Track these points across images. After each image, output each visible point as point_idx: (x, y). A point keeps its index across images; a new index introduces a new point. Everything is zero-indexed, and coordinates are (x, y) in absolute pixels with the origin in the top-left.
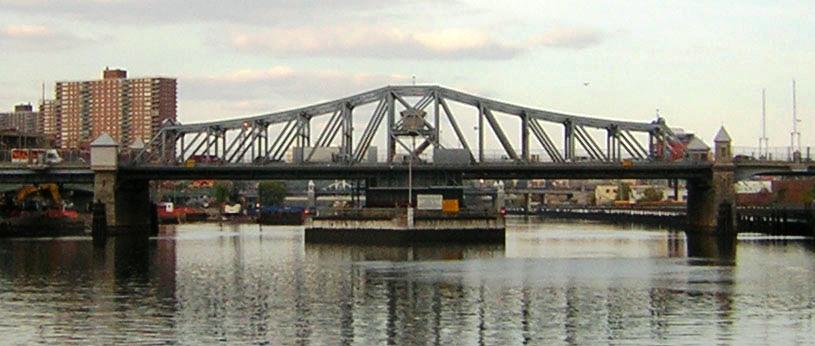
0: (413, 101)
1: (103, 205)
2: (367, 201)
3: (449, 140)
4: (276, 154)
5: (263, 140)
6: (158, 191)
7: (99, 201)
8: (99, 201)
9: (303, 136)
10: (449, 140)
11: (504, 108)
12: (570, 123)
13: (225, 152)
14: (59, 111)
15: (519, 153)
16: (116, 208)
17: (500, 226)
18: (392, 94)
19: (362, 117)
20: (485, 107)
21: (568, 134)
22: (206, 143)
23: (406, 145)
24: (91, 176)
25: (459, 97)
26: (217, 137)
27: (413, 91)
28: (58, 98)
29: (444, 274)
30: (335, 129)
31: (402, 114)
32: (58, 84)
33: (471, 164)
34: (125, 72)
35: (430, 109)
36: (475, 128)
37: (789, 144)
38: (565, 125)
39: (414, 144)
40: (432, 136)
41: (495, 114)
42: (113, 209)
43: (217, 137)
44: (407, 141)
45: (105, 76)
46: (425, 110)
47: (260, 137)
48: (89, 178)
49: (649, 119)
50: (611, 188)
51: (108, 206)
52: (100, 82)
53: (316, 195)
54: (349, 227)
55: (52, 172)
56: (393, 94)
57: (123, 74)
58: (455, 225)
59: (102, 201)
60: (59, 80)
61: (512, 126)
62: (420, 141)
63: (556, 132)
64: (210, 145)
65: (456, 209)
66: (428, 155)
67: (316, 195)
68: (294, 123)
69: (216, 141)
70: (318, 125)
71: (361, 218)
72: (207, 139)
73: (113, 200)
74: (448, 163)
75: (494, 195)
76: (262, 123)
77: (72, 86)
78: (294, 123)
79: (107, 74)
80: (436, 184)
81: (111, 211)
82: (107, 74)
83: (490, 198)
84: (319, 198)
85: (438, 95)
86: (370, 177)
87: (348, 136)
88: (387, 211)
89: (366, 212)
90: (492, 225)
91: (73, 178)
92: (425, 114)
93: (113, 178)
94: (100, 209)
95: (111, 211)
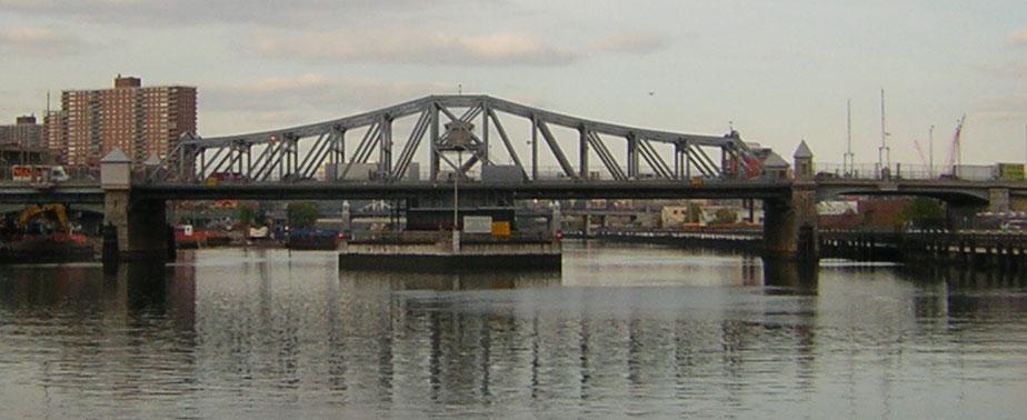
0: (459, 112)
3: (499, 155)
5: (292, 155)
7: (110, 223)
8: (110, 223)
9: (337, 152)
10: (499, 155)
11: (560, 120)
12: (634, 136)
13: (250, 169)
15: (577, 170)
16: (129, 230)
17: (556, 251)
19: (402, 130)
20: (539, 119)
23: (451, 161)
24: (102, 196)
25: (510, 108)
26: (241, 152)
27: (458, 101)
28: (64, 109)
31: (447, 126)
32: (65, 93)
34: (139, 80)
35: (478, 121)
38: (629, 139)
39: (460, 160)
40: (481, 151)
42: (126, 232)
43: (241, 152)
44: (453, 157)
45: (117, 85)
46: (472, 122)
47: (289, 152)
48: (99, 198)
49: (721, 132)
53: (352, 217)
54: (388, 252)
55: (58, 191)
56: (436, 104)
57: (136, 82)
58: (506, 250)
60: (65, 89)
61: (569, 140)
62: (466, 157)
63: (618, 147)
64: (234, 161)
65: (507, 232)
66: (476, 171)
67: (352, 217)
68: (326, 136)
70: (353, 139)
71: (401, 243)
72: (230, 155)
73: (125, 222)
74: (498, 182)
75: (550, 217)
76: (292, 137)
77: (81, 95)
78: (326, 136)
79: (119, 82)
80: (485, 205)
81: (123, 235)
82: (119, 82)
83: (544, 219)
85: (487, 105)
88: (431, 235)
90: (547, 250)
91: (82, 198)
93: (125, 198)
94: (111, 234)
95: (123, 235)
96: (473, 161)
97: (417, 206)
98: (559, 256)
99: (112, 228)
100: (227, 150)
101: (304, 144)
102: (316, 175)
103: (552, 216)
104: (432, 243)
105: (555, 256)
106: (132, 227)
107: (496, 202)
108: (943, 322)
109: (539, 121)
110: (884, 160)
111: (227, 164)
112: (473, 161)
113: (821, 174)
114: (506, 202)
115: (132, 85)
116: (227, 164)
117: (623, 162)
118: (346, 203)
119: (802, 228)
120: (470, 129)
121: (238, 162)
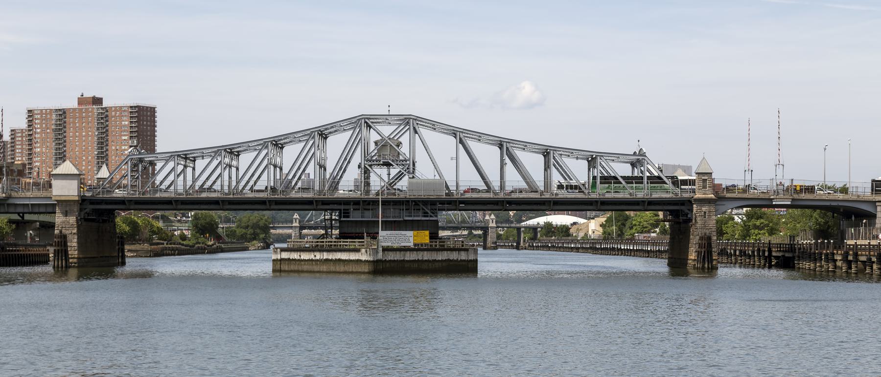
0: (387, 130)
1: (65, 237)
2: (340, 233)
3: (425, 171)
4: (230, 182)
5: (234, 169)
6: (122, 220)
7: (61, 232)
8: (61, 232)
9: (275, 166)
10: (425, 171)
11: (479, 137)
12: (548, 153)
13: (238, 182)
14: (30, 140)
15: (541, 185)
16: (78, 239)
17: (471, 257)
18: (366, 122)
19: (336, 144)
20: (460, 136)
21: (547, 167)
22: (172, 175)
23: (379, 178)
24: (54, 205)
25: (433, 125)
26: (185, 166)
27: (386, 119)
28: (29, 126)
29: (246, 195)
30: (307, 160)
31: (376, 143)
32: (30, 111)
33: (447, 194)
34: (101, 99)
35: (405, 139)
36: (452, 159)
37: (267, 185)
38: (545, 156)
39: (389, 174)
40: (409, 167)
41: (472, 144)
42: (76, 240)
43: (185, 166)
44: (383, 171)
45: (79, 104)
46: (400, 140)
47: (230, 166)
48: (50, 209)
49: (630, 149)
50: (341, 192)
51: (69, 237)
52: (74, 109)
53: (302, 228)
54: (318, 257)
55: (11, 201)
56: (367, 122)
57: (97, 101)
58: (426, 256)
59: (63, 231)
60: (31, 108)
61: (488, 156)
62: (394, 171)
63: (534, 163)
64: (178, 176)
65: (427, 240)
66: (403, 184)
67: (302, 228)
68: (264, 152)
69: (183, 171)
70: (290, 154)
71: (330, 250)
72: (173, 169)
73: (75, 231)
74: (422, 194)
75: (485, 229)
76: (233, 151)
77: (45, 113)
78: (264, 152)
79: (82, 101)
80: (410, 216)
81: (73, 243)
82: (82, 101)
83: (480, 232)
84: (305, 231)
85: (410, 122)
86: (342, 207)
87: (321, 167)
88: (356, 243)
89: (342, 243)
90: (463, 256)
91: (35, 209)
92: (399, 144)
93: (76, 208)
94: (63, 240)
95: (73, 243)
96: (400, 176)
97: (348, 217)
98: (476, 261)
99: (63, 238)
100: (171, 165)
101: (245, 159)
102: (217, 187)
103: (487, 228)
104: (357, 250)
105: (471, 261)
106: (80, 234)
107: (421, 212)
108: (73, 272)
109: (460, 139)
110: (779, 177)
111: (171, 178)
112: (400, 176)
113: (64, 161)
114: (430, 213)
115: (93, 104)
116: (171, 178)
117: (538, 177)
118: (296, 216)
119: (701, 238)
120: (398, 146)
121: (182, 176)
